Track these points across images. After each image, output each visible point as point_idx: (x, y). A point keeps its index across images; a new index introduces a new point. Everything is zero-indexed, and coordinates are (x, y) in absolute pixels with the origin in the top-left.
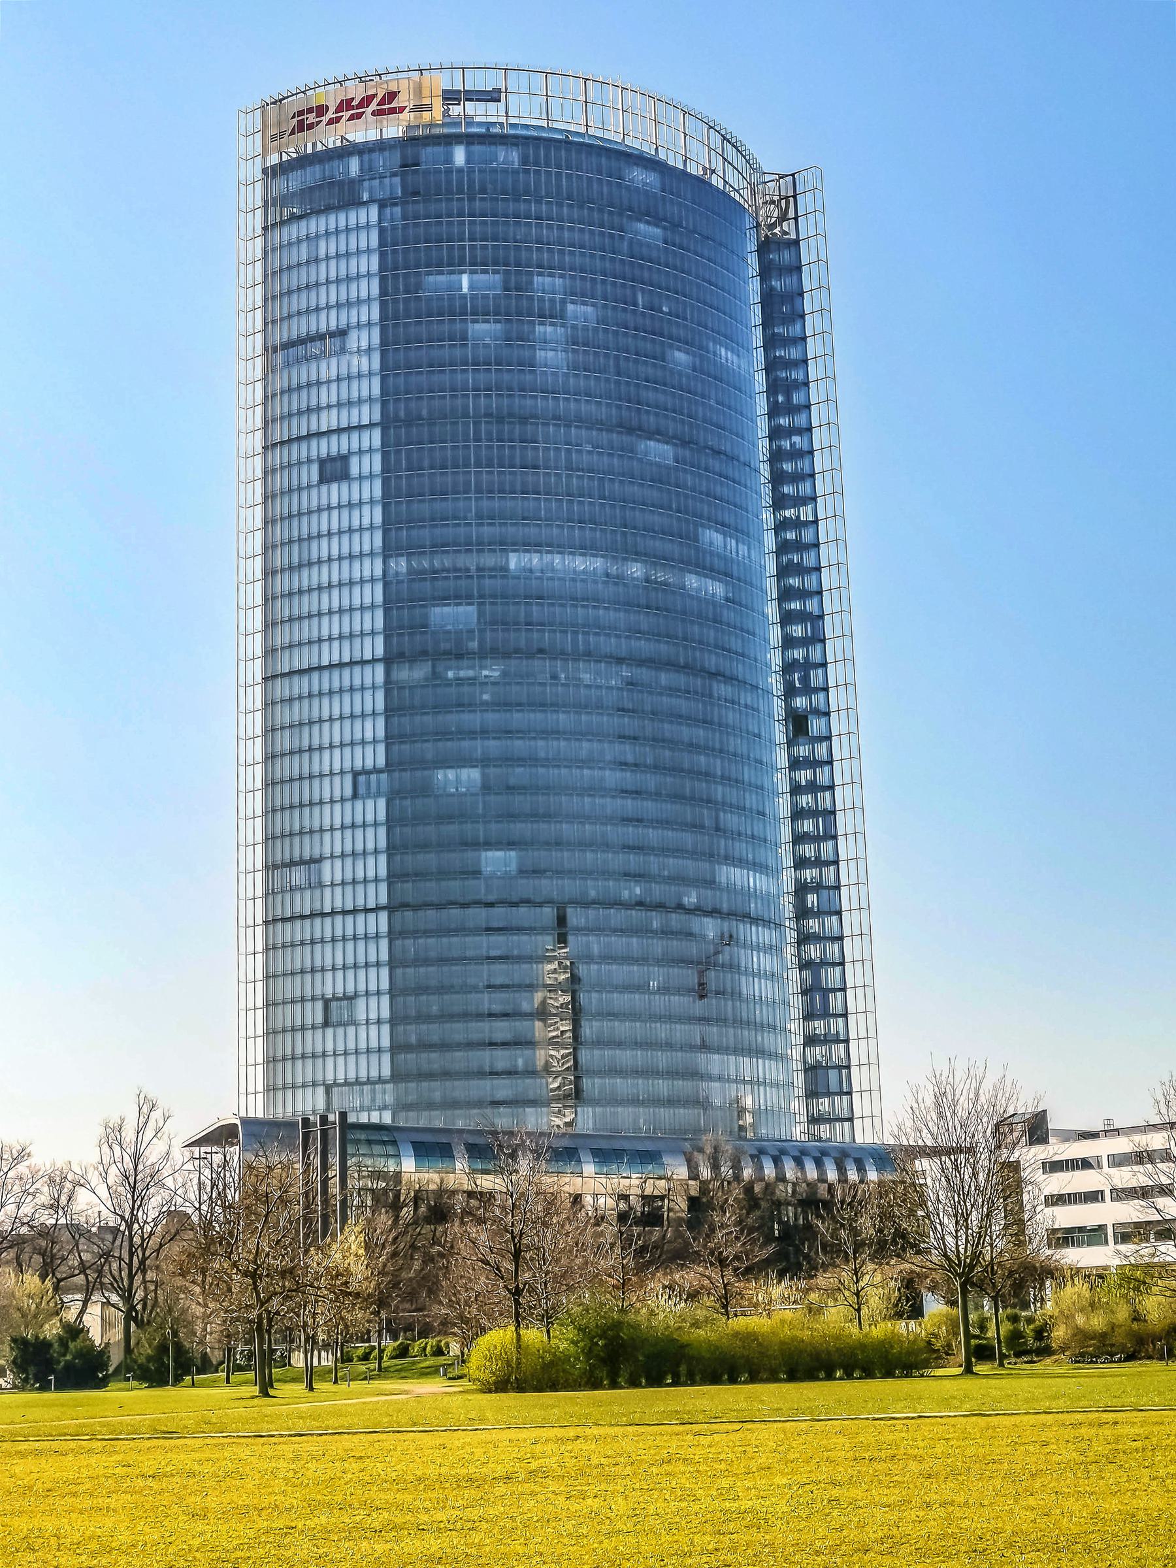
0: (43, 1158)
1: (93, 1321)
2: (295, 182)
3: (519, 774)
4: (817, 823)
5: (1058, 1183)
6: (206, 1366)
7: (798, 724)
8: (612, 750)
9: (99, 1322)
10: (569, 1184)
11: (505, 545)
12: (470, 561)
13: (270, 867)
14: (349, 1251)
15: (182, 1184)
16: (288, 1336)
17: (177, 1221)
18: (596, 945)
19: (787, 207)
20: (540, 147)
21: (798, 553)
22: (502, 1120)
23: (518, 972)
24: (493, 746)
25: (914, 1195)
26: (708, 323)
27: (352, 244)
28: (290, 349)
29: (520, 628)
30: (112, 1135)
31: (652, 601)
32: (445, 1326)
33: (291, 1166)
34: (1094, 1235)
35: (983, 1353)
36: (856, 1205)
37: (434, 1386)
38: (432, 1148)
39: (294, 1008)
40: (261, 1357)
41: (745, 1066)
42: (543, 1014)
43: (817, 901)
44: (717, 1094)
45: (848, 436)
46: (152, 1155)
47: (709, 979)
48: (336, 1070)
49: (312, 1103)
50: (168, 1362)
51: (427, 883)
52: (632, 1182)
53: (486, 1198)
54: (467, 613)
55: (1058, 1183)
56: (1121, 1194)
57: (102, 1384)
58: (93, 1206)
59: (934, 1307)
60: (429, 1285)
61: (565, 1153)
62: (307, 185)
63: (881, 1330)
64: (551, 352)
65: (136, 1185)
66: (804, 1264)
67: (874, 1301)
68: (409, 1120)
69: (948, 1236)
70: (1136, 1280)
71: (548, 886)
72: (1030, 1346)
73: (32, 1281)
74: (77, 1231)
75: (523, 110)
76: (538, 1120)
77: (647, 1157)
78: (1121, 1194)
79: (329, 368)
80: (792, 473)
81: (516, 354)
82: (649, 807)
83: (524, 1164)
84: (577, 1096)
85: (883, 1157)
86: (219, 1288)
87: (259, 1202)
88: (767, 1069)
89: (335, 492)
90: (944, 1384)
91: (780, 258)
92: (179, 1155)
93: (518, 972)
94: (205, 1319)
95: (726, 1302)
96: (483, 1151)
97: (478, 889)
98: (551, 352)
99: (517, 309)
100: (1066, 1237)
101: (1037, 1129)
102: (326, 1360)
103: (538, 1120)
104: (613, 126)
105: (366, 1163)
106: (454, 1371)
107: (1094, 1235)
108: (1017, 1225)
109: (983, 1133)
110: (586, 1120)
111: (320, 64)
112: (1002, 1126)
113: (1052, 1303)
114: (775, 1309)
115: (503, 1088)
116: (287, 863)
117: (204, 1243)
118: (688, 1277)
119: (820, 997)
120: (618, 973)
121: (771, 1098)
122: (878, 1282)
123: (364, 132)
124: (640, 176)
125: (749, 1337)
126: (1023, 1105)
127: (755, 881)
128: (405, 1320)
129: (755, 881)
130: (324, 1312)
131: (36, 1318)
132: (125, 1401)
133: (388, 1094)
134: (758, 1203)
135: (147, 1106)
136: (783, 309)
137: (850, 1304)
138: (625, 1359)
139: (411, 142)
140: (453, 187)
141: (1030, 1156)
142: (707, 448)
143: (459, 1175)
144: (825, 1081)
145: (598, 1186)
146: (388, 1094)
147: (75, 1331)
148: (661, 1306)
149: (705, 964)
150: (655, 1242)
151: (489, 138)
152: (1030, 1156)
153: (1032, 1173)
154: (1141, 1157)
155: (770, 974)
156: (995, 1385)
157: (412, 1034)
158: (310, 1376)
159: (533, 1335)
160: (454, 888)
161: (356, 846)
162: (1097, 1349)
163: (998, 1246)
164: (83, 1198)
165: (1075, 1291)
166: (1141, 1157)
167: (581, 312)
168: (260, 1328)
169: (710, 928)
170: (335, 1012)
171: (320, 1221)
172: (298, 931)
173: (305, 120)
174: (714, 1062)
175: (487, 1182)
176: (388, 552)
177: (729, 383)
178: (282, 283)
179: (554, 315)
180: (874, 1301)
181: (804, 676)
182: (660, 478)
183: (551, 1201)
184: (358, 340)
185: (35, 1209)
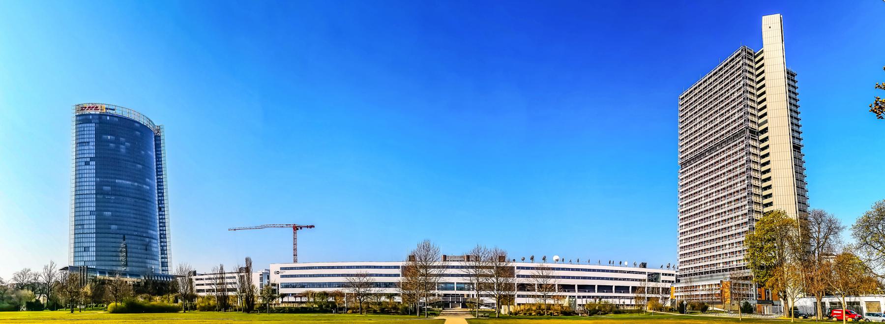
0: (33, 271)
1: (41, 299)
2: (81, 118)
3: (118, 214)
4: (163, 225)
5: (197, 282)
6: (62, 307)
7: (160, 209)
8: (132, 211)
9: (43, 299)
10: (125, 279)
11: (116, 178)
12: (110, 180)
13: (75, 225)
14: (87, 289)
15: (58, 276)
16: (77, 303)
17: (57, 283)
18: (130, 241)
19: (158, 131)
20: (121, 118)
21: (160, 182)
22: (114, 268)
23: (117, 245)
24: (113, 209)
25: (176, 283)
26: (146, 148)
27: (91, 128)
28: (80, 144)
29: (117, 191)
30: (46, 268)
31: (139, 189)
32: (104, 302)
33: (77, 274)
34: (203, 291)
35: (186, 309)
36: (169, 284)
37: (102, 312)
38: (102, 272)
39: (79, 248)
40: (72, 305)
41: (153, 262)
42: (121, 252)
43: (163, 236)
44: (149, 266)
45: (166, 141)
46: (53, 271)
47: (147, 247)
48: (86, 259)
49: (82, 264)
50: (54, 306)
51: (102, 230)
52: (135, 279)
53: (111, 281)
54: (109, 188)
55: (197, 282)
56: (207, 284)
57: (42, 310)
58: (42, 279)
59: (180, 301)
60: (101, 295)
61: (124, 274)
62: (83, 119)
63: (172, 305)
64: (123, 149)
65: (50, 276)
66: (161, 290)
67: (171, 300)
68: (99, 267)
69: (182, 290)
70: (209, 298)
71: (122, 231)
72: (193, 308)
73: (30, 292)
74: (39, 283)
75: (118, 112)
76: (119, 269)
77: (137, 275)
78: (207, 284)
79: (87, 148)
80: (159, 171)
81: (117, 149)
82: (138, 221)
83: (117, 276)
84: (126, 265)
85: (173, 277)
86: (64, 294)
87: (72, 280)
88: (156, 262)
89: (87, 167)
90: (181, 314)
91: (158, 138)
92: (58, 272)
93: (117, 245)
94: (62, 300)
95: (150, 299)
96: (112, 273)
97: (111, 231)
98: (123, 149)
99: (117, 142)
100: (199, 291)
101: (195, 273)
102: (83, 307)
103: (119, 269)
104: (132, 117)
105: (91, 275)
106: (105, 309)
107: (203, 291)
108: (192, 288)
109: (187, 273)
110: (128, 269)
111: (86, 101)
112: (190, 272)
113: (197, 301)
114: (157, 300)
115: (114, 263)
116: (79, 225)
117: (62, 287)
118: (144, 295)
119: (163, 251)
120: (133, 246)
121: (156, 267)
122: (172, 297)
123: (93, 112)
124: (137, 124)
125: (153, 305)
126: (193, 270)
127: (154, 233)
128: (97, 299)
129: (154, 233)
130: (83, 299)
131: (31, 298)
132: (47, 313)
133: (95, 263)
134: (155, 283)
135: (52, 263)
136: (158, 146)
137: (169, 301)
138: (133, 308)
139: (100, 115)
140: (107, 122)
141: (194, 278)
142: (147, 167)
143: (107, 277)
144: (164, 264)
145: (129, 280)
146: (95, 263)
147: (38, 301)
148: (140, 299)
149: (147, 245)
150: (138, 289)
151: (112, 116)
152: (194, 278)
153: (194, 280)
154: (210, 279)
155: (156, 247)
156: (188, 314)
157: (99, 253)
158: (80, 310)
159: (119, 304)
160: (107, 231)
161: (91, 223)
162: (203, 309)
163: (189, 292)
164: (40, 278)
165: (200, 300)
166: (210, 279)
167: (127, 144)
168: (72, 301)
169: (147, 240)
170: (86, 249)
171: (83, 283)
172: (80, 236)
173: (83, 109)
174: (148, 261)
175: (112, 278)
176: (96, 177)
177: (149, 156)
178: (79, 133)
179: (124, 144)
180: (171, 300)
181: (161, 201)
182: (140, 170)
183: (122, 282)
184: (91, 144)
185: (31, 279)
